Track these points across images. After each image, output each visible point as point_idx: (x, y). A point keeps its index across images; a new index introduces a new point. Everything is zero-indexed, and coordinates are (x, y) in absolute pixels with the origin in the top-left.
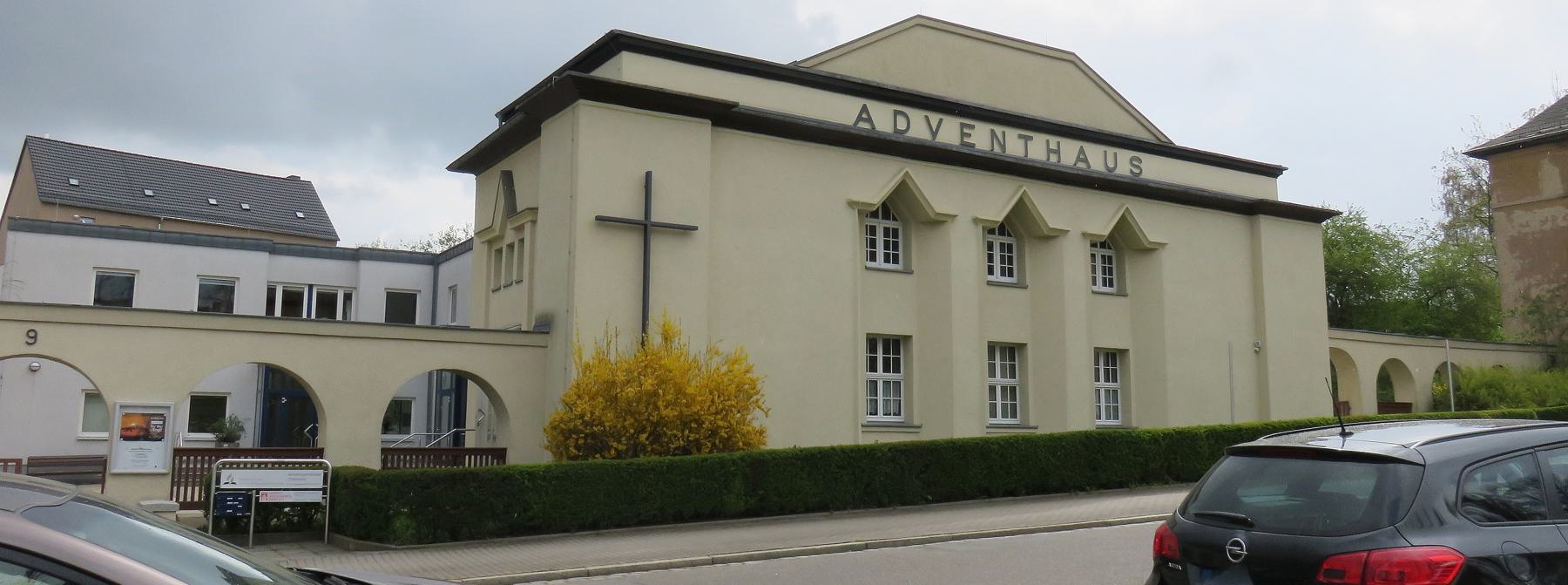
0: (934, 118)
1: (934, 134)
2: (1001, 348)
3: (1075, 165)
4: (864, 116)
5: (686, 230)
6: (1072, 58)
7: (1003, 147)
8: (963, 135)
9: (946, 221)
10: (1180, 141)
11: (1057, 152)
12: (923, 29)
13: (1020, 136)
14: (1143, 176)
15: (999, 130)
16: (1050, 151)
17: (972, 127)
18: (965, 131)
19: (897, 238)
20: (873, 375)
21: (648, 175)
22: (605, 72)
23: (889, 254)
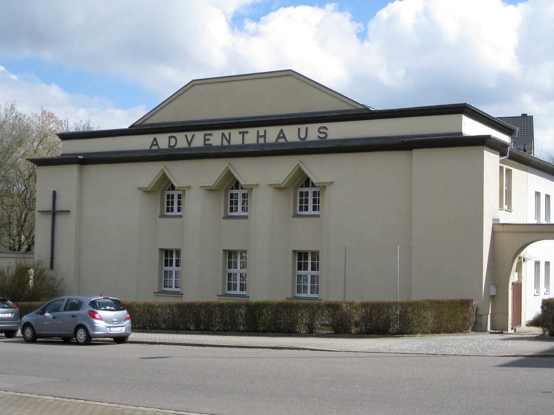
0: (190, 135)
1: (189, 143)
2: (312, 253)
3: (276, 141)
4: (282, 135)
5: (331, 183)
6: (290, 73)
7: (229, 141)
8: (205, 140)
9: (312, 182)
10: (376, 105)
11: (264, 136)
12: (197, 86)
13: (240, 133)
14: (329, 138)
15: (226, 132)
16: (258, 136)
17: (211, 134)
18: (207, 137)
19: (167, 207)
20: (244, 271)
21: (54, 193)
22: (189, 140)
23: (318, 197)
